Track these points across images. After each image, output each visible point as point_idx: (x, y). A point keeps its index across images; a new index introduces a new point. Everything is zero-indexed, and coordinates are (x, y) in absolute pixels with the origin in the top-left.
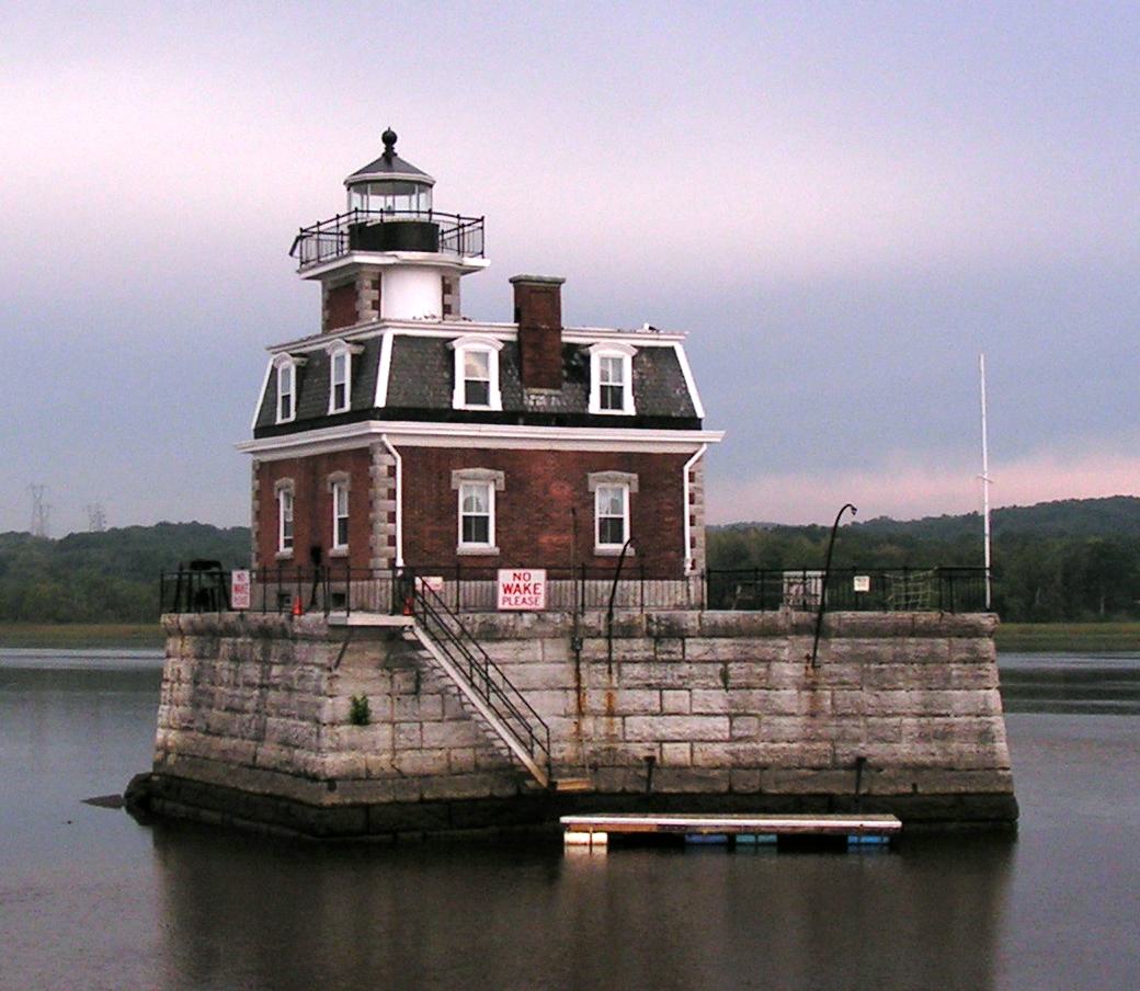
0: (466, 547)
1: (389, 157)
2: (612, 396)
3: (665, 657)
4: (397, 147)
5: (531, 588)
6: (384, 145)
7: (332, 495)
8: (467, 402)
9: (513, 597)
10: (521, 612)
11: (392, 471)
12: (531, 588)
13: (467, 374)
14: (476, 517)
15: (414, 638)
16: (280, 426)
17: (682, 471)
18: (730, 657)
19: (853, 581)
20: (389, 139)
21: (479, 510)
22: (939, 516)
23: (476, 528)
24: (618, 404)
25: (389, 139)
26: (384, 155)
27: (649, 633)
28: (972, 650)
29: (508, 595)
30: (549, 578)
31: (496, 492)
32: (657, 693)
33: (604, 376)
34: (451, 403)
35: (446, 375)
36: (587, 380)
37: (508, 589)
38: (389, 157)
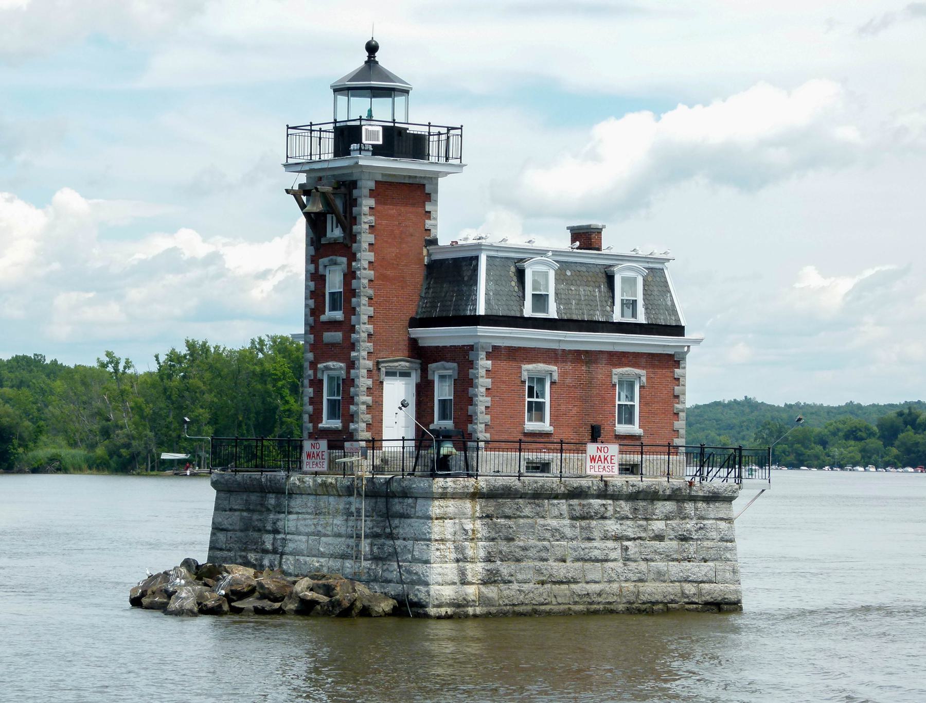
0: (531, 426)
1: (371, 62)
4: (378, 56)
5: (609, 459)
6: (367, 54)
7: (433, 381)
8: (534, 310)
9: (596, 465)
12: (609, 459)
13: (534, 289)
14: (536, 402)
20: (372, 48)
21: (537, 397)
23: (627, 414)
24: (545, 309)
25: (372, 48)
26: (366, 62)
28: (246, 557)
29: (593, 464)
30: (621, 452)
33: (536, 285)
34: (522, 311)
37: (593, 459)
38: (371, 62)
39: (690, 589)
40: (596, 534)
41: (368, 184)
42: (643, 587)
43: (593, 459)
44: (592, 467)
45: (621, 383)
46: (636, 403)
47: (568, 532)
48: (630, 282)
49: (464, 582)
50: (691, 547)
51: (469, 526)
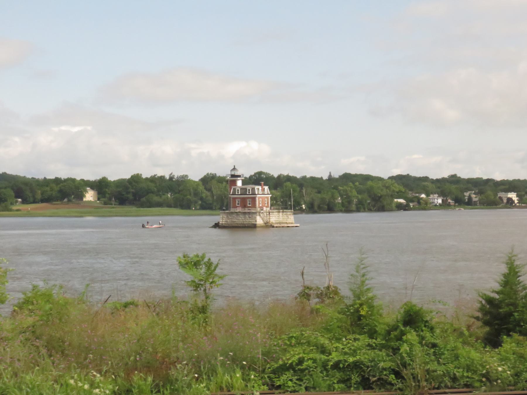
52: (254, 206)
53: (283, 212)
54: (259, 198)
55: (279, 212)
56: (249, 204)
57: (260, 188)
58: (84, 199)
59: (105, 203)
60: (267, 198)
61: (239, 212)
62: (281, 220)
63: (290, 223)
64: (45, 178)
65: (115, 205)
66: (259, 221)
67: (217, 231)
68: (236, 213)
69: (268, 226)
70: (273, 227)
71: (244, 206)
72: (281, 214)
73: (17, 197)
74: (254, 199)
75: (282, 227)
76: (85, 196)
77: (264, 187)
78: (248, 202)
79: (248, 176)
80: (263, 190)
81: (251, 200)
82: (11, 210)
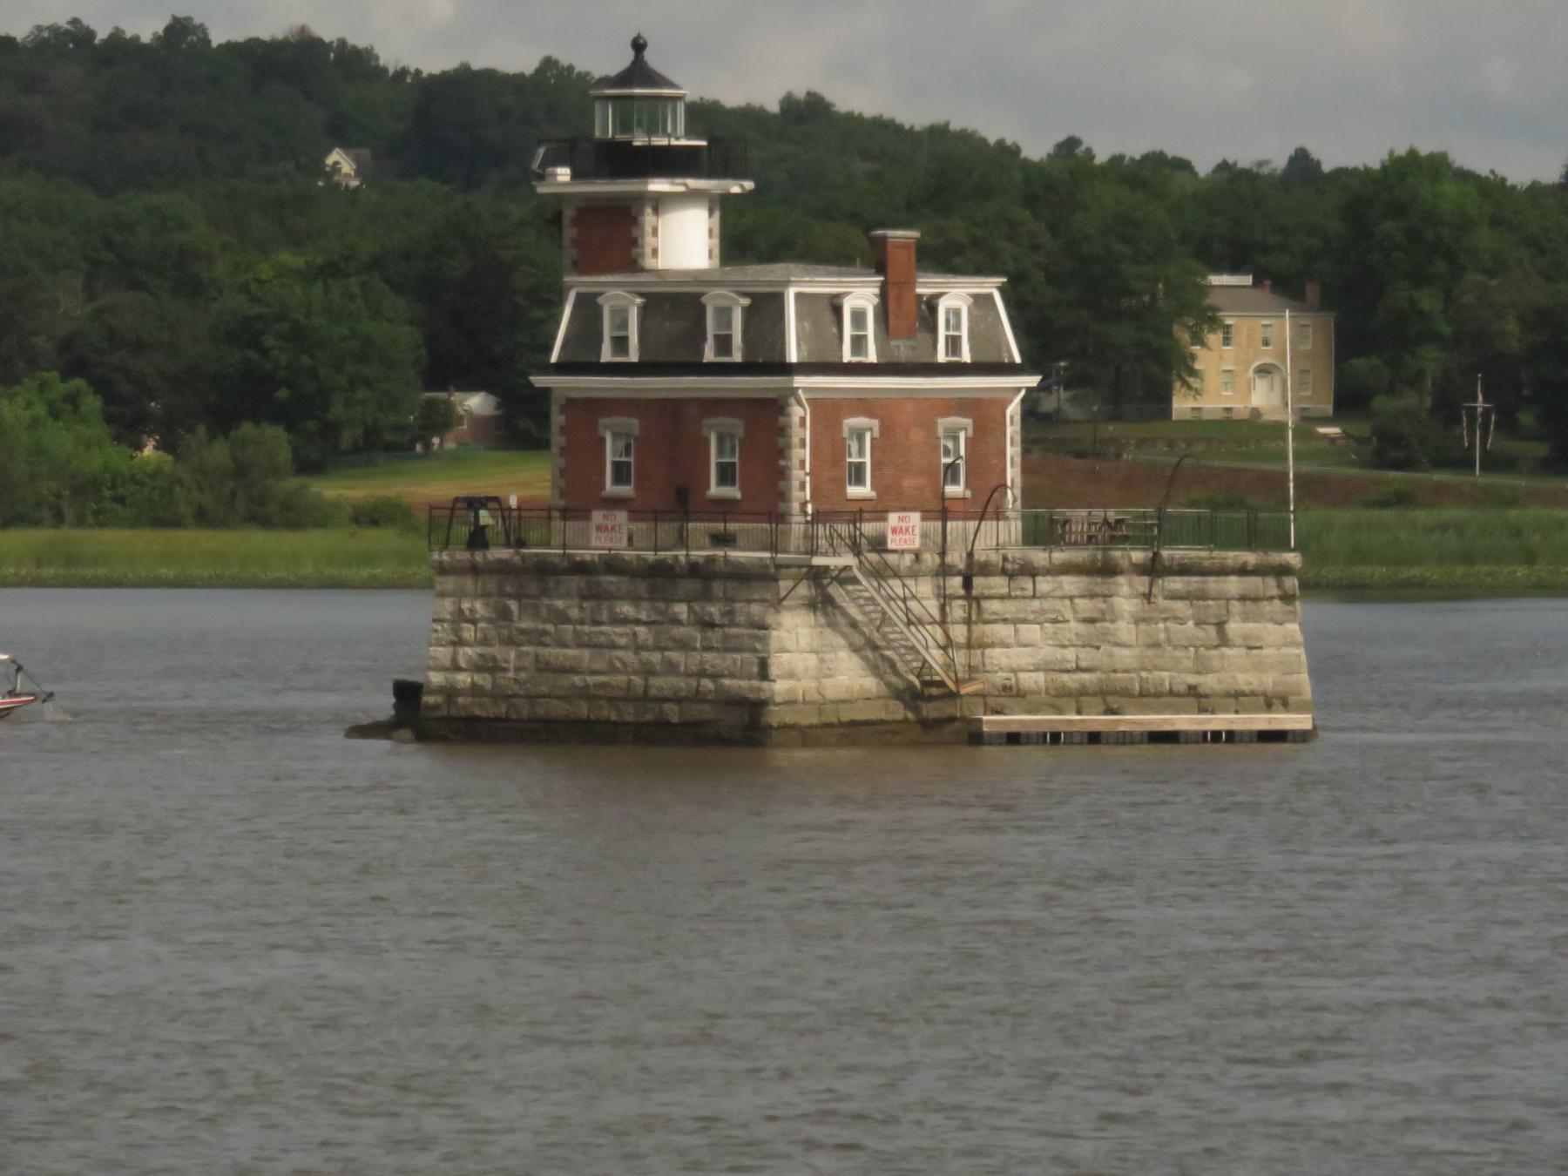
2: (954, 344)
3: (1019, 593)
10: (903, 552)
11: (803, 420)
15: (1023, 392)
16: (849, 364)
17: (1004, 415)
18: (1075, 593)
19: (979, 270)
20: (639, 46)
22: (146, 28)
25: (639, 46)
27: (1004, 572)
31: (873, 439)
32: (1011, 627)
35: (835, 330)
36: (934, 330)
37: (599, 528)
39: (708, 684)
40: (741, 619)
41: (569, 213)
42: (656, 682)
43: (599, 528)
44: (598, 538)
45: (851, 434)
46: (867, 459)
47: (574, 613)
48: (724, 314)
49: (457, 668)
50: (715, 636)
51: (466, 605)
52: (767, 501)
53: (1153, 569)
54: (828, 411)
55: (1108, 570)
56: (726, 475)
57: (861, 295)
58: (1182, 405)
59: (1389, 449)
60: (984, 412)
61: (612, 565)
62: (1125, 656)
63: (1237, 698)
64: (1301, 159)
65: (1493, 463)
66: (807, 662)
67: (411, 763)
68: (581, 568)
69: (931, 720)
70: (976, 738)
71: (678, 501)
72: (1125, 595)
73: (450, 370)
74: (766, 417)
75: (1105, 741)
76: (1186, 367)
77: (926, 286)
78: (702, 451)
79: (1138, 157)
80: (907, 317)
81: (736, 426)
82: (295, 516)
